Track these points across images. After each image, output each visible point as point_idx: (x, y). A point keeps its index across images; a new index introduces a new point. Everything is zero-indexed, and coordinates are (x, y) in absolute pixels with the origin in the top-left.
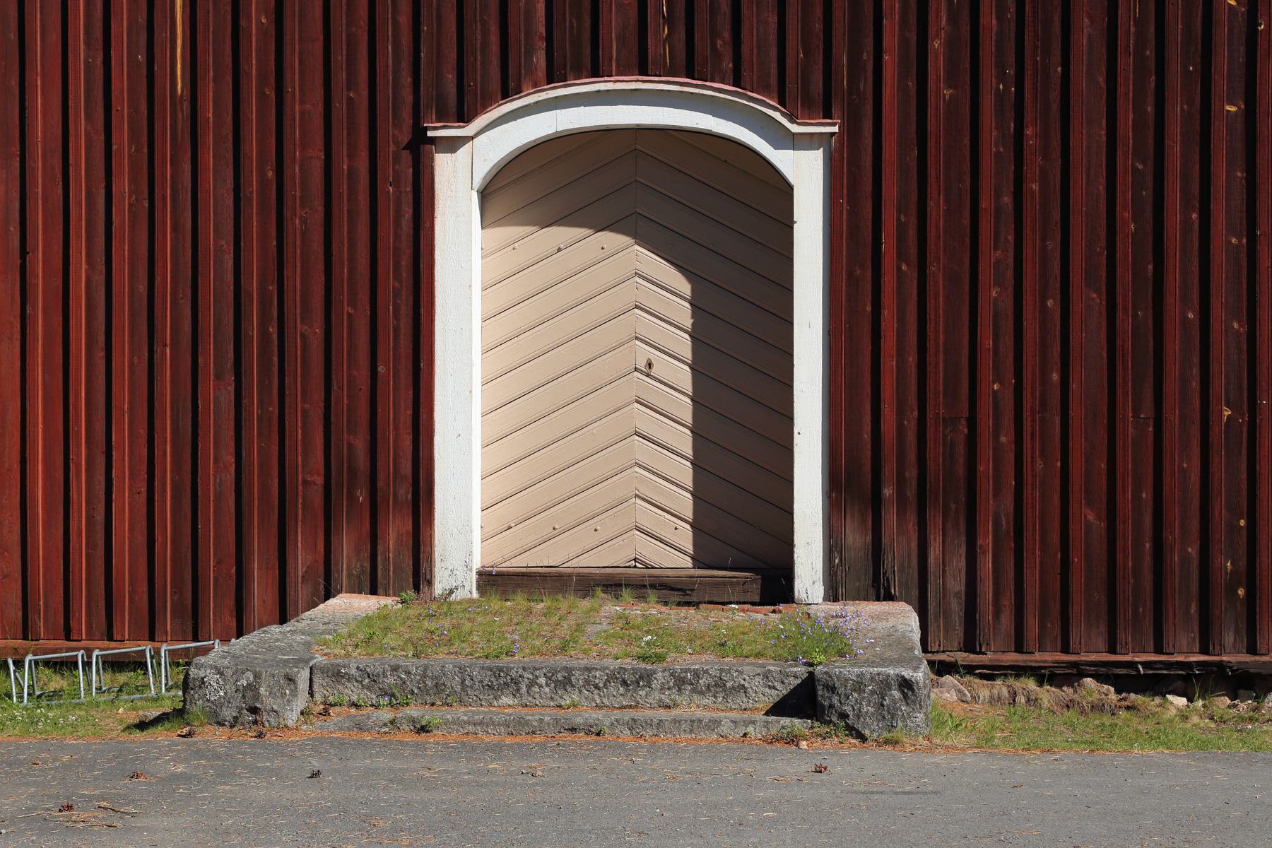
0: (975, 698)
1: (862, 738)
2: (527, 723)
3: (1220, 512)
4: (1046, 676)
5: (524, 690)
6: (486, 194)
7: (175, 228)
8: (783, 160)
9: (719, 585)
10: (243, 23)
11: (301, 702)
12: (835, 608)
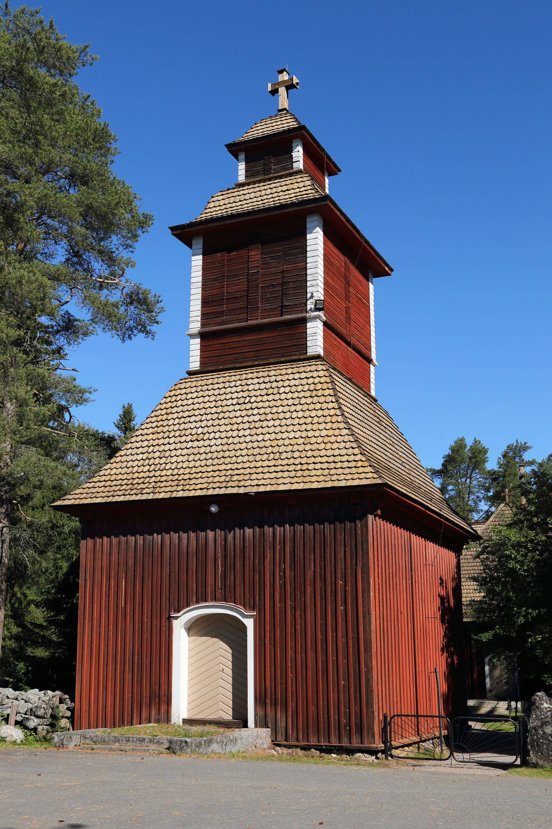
4: (304, 748)
7: (121, 638)
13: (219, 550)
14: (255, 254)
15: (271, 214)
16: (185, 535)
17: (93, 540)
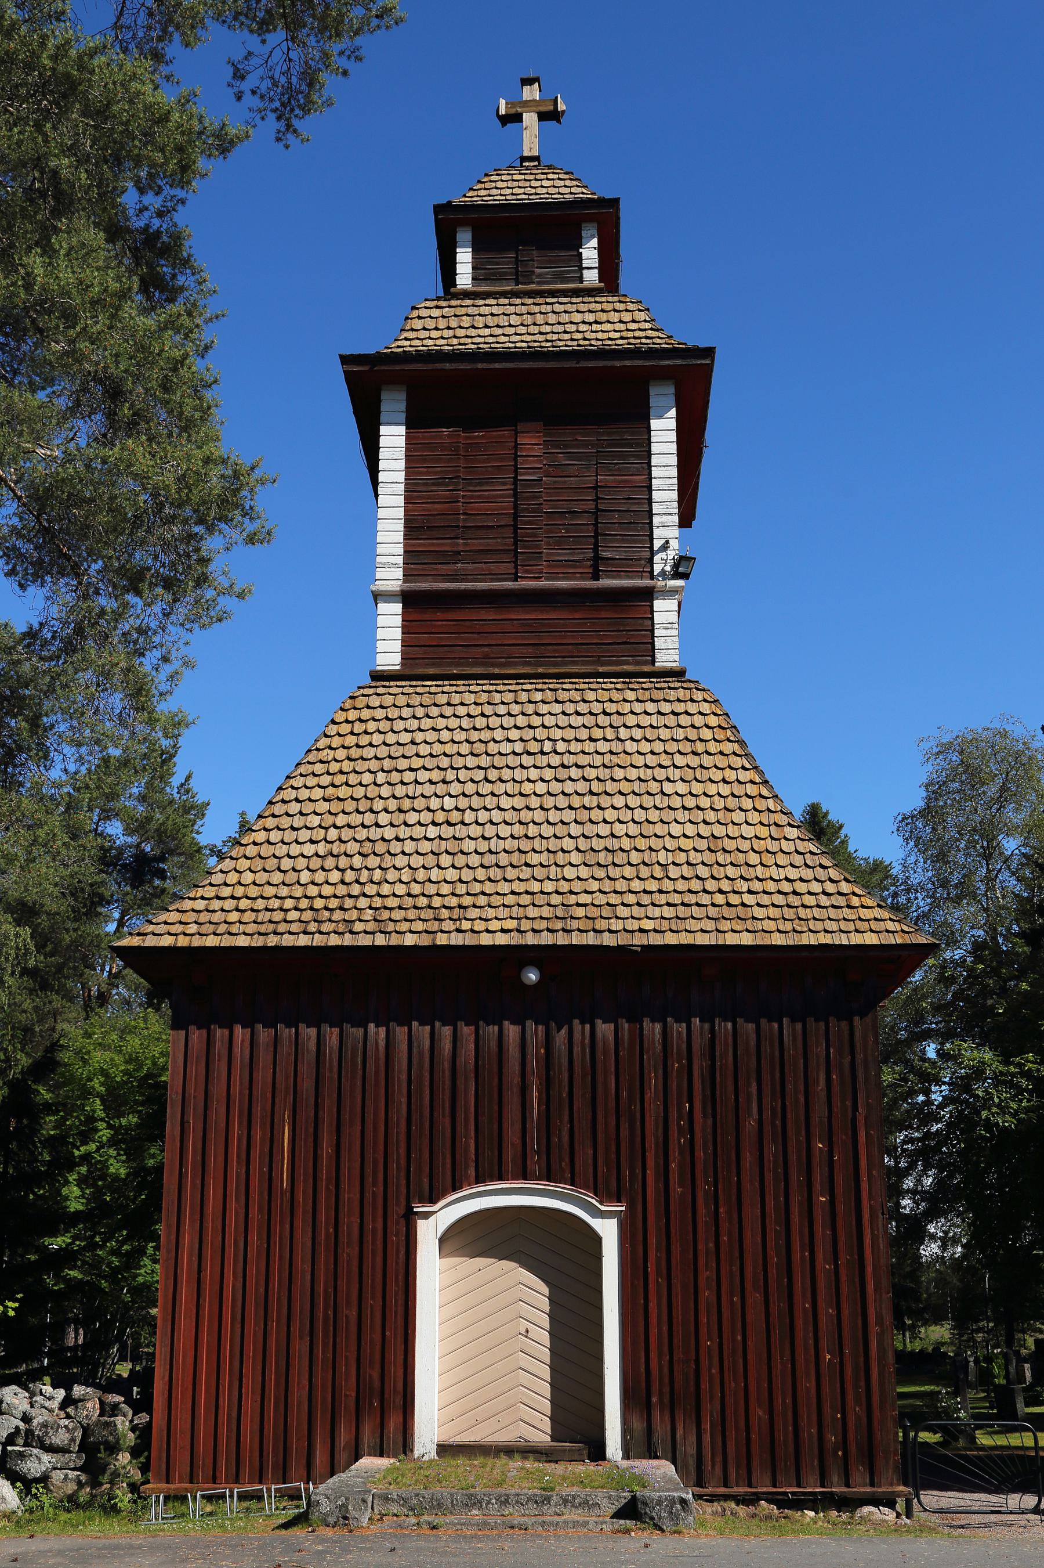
0: (704, 1512)
1: (663, 1531)
2: (489, 1524)
3: (827, 1409)
4: (740, 1500)
5: (484, 1506)
6: (441, 1241)
7: (281, 1257)
8: (596, 1224)
9: (563, 1451)
10: (319, 1152)
11: (368, 1514)
12: (631, 1463)
13: (533, 1066)
14: (532, 443)
15: (583, 364)
16: (447, 1031)
17: (204, 1032)
